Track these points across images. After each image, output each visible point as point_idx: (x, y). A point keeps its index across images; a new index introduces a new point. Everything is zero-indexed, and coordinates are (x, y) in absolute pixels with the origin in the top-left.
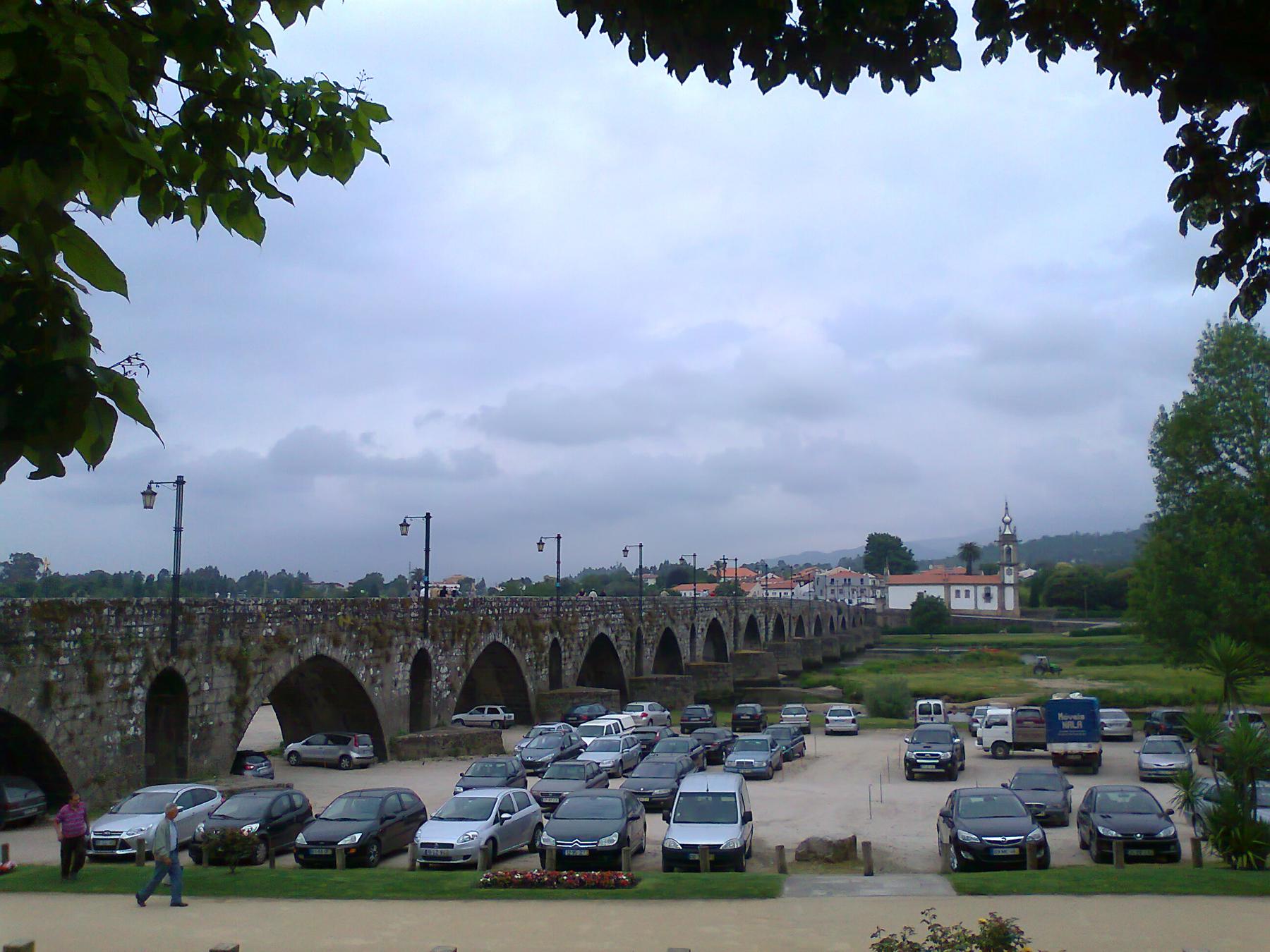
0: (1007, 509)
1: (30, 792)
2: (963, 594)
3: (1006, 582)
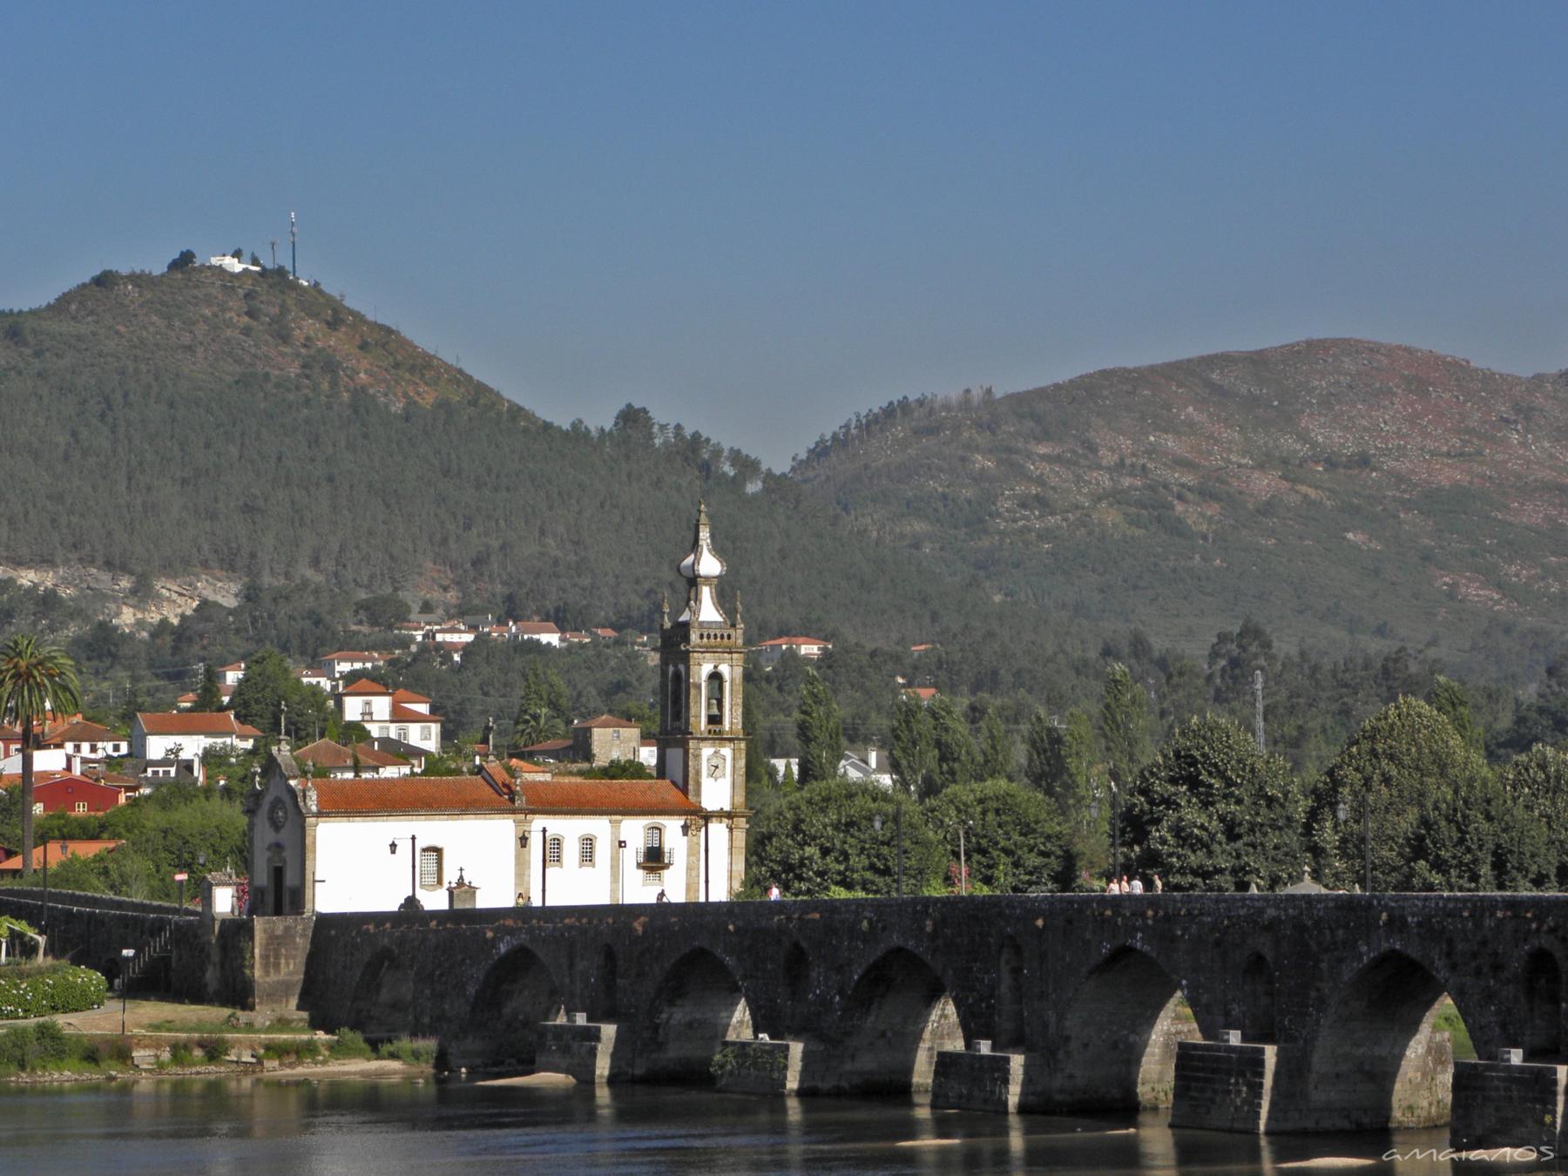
2: (571, 851)
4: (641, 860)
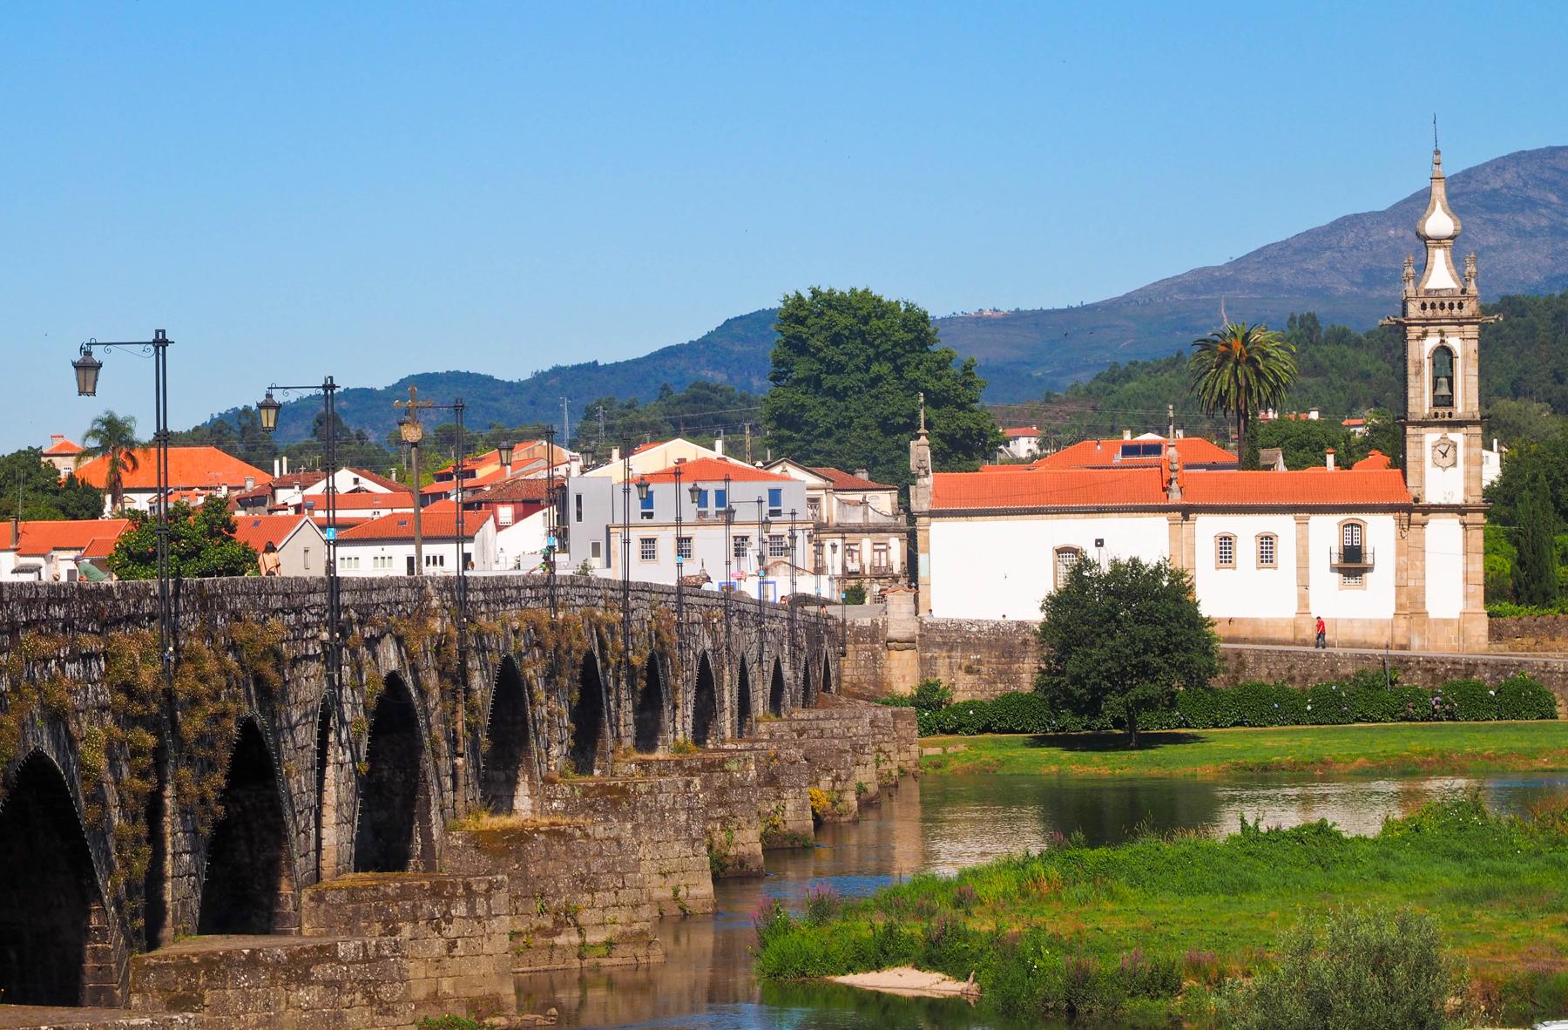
0: (1437, 152)
1: (1218, 640)
2: (1246, 550)
3: (1431, 498)
4: (1336, 561)
